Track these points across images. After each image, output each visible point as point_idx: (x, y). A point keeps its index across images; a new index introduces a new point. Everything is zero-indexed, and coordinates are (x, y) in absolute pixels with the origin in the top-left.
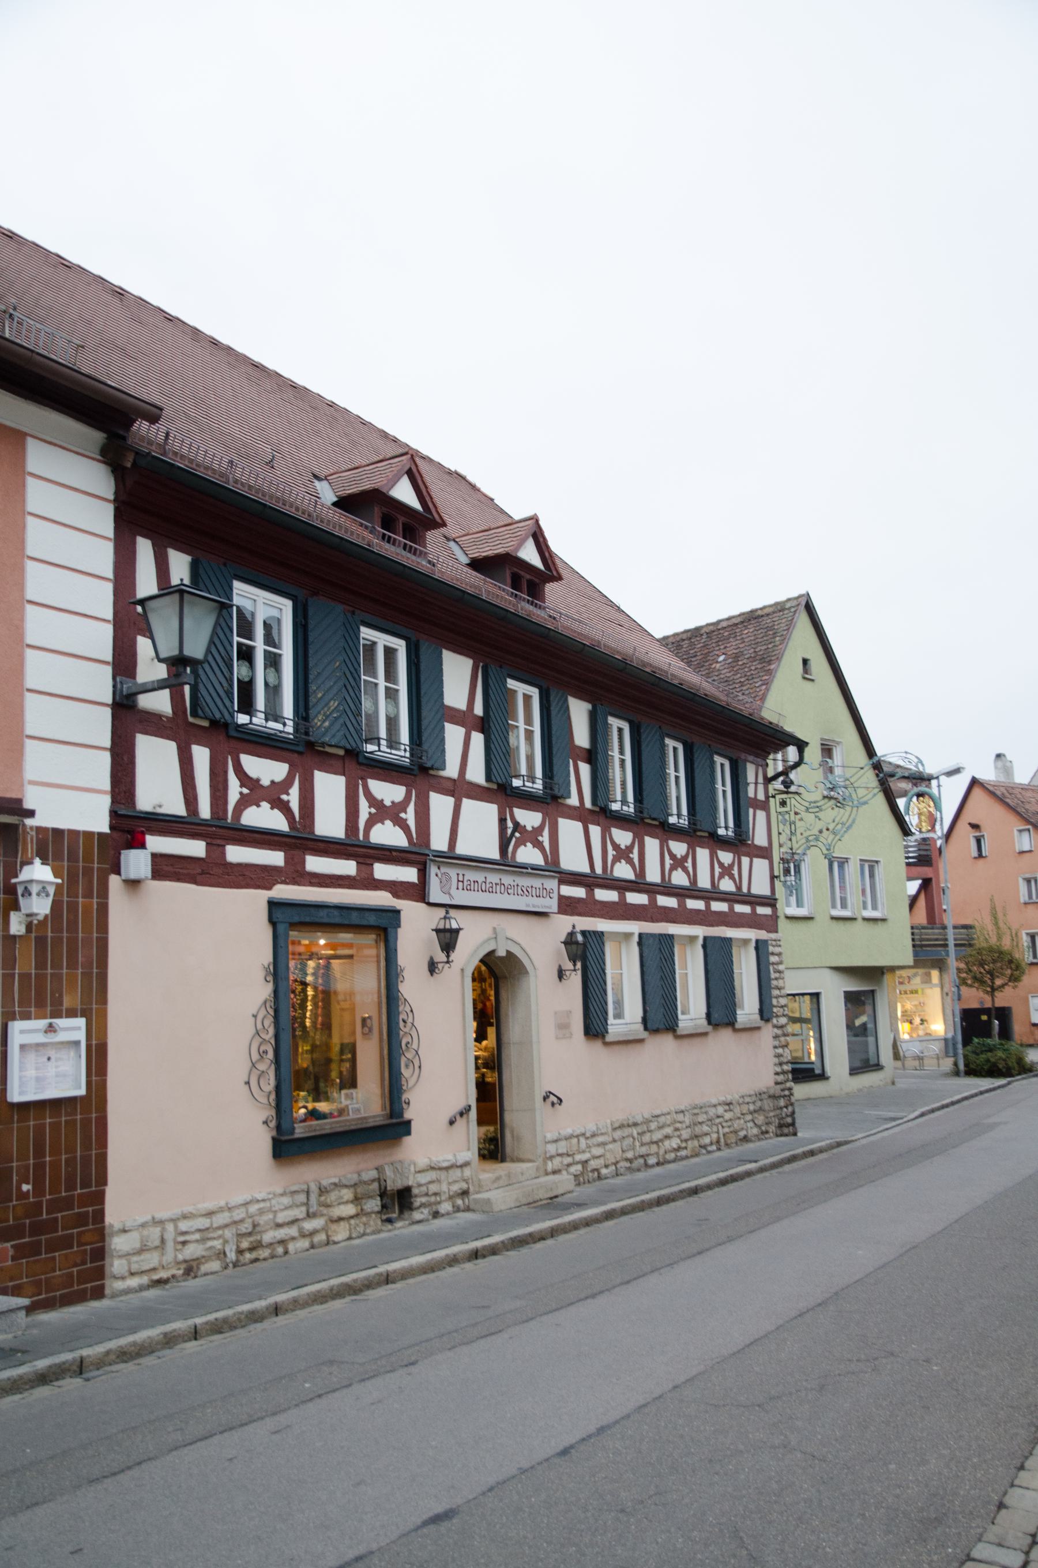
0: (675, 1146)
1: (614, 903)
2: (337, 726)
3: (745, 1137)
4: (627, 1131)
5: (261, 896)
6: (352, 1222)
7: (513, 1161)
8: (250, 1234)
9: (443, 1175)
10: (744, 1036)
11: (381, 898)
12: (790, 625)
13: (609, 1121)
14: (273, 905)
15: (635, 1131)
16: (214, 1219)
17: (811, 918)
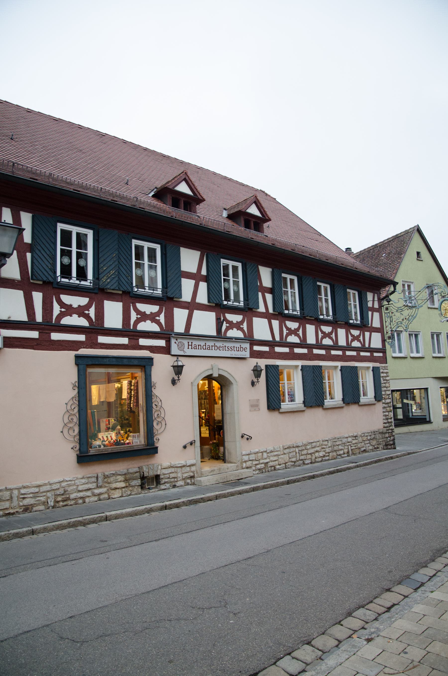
0: (322, 455)
1: (287, 353)
2: (114, 281)
3: (364, 450)
4: (292, 450)
5: (72, 354)
6: (124, 489)
7: (228, 463)
9: (179, 470)
10: (365, 408)
11: (145, 353)
12: (410, 239)
13: (281, 446)
14: (77, 357)
15: (297, 450)
17: (423, 358)
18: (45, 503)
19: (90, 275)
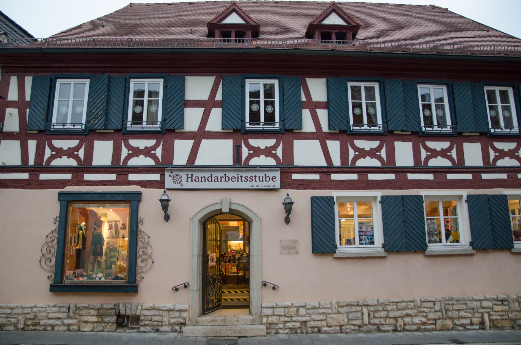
6: (96, 324)
8: (33, 319)
13: (334, 302)
16: (14, 310)
18: (15, 325)
19: (277, 119)
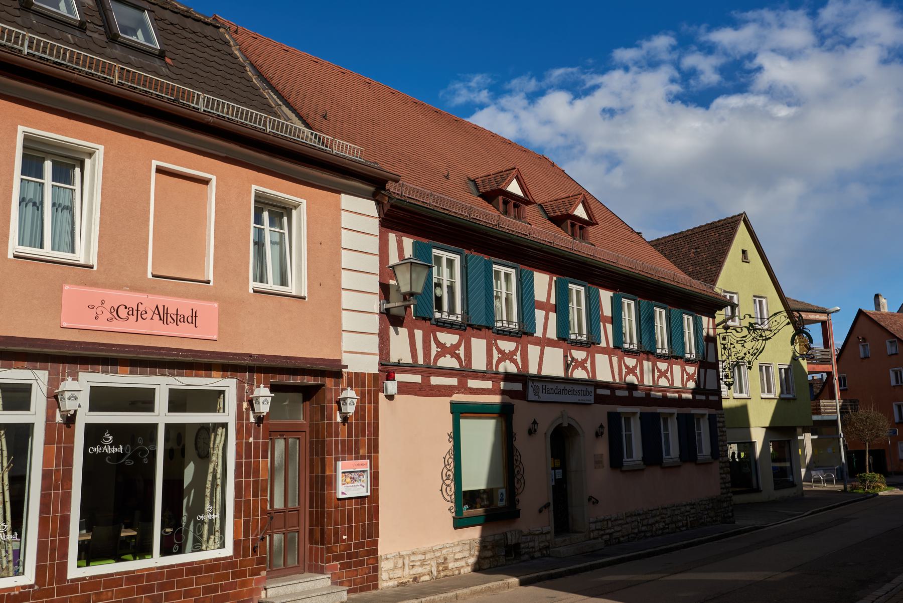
1: (607, 396)
4: (634, 518)
5: (447, 400)
14: (451, 403)
19: (458, 310)
